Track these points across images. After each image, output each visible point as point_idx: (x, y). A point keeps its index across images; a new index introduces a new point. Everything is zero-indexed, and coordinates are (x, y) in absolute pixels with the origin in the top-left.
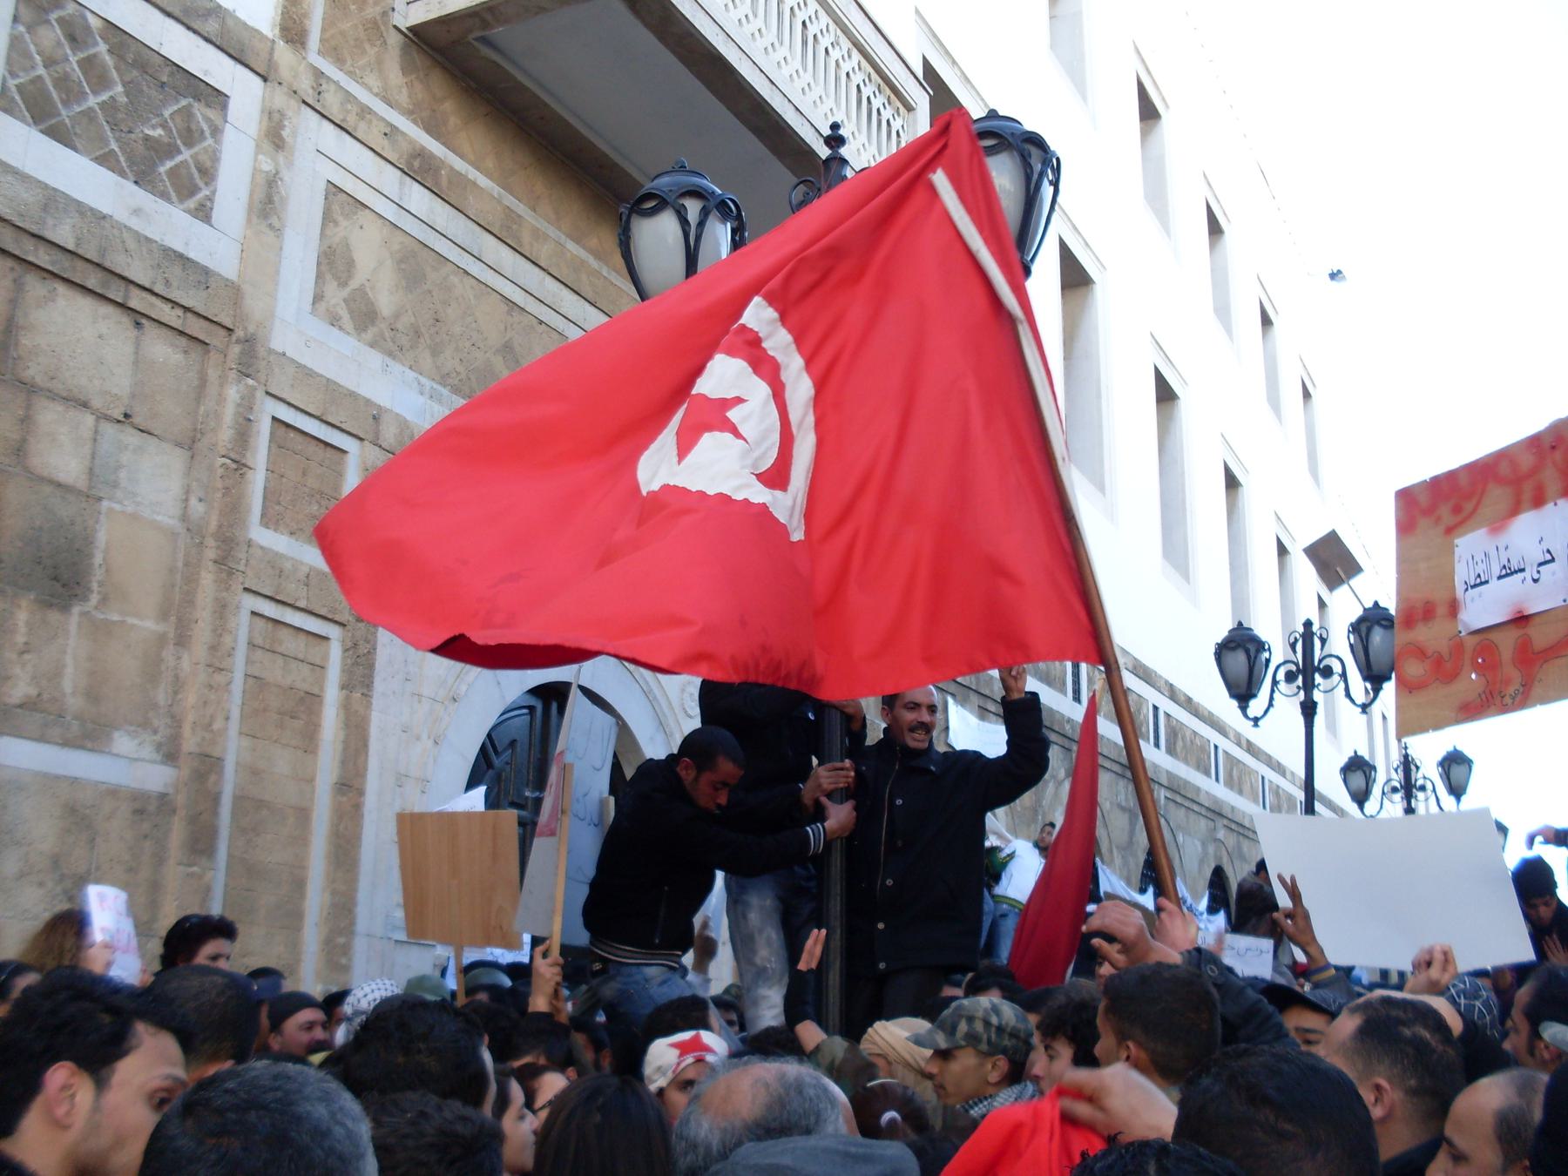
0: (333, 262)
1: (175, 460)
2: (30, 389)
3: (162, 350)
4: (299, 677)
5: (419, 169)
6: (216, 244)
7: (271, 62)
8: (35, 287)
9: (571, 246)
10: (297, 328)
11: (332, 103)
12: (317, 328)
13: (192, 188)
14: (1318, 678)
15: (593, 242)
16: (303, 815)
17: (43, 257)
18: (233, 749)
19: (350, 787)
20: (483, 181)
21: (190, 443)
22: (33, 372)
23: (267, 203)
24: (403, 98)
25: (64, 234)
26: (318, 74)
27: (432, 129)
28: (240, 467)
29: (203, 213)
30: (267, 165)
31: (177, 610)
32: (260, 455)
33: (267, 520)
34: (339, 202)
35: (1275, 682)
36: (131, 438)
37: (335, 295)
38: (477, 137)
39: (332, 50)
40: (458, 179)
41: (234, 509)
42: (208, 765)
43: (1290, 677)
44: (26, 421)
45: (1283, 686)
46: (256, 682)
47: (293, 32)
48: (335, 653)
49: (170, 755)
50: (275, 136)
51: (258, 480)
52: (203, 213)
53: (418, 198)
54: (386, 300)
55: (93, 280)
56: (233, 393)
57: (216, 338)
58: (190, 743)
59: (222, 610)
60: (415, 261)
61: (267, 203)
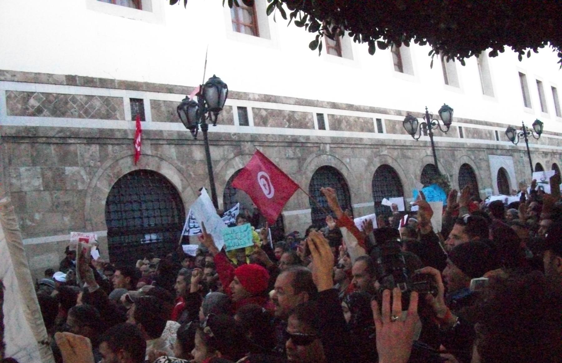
45: (520, 137)
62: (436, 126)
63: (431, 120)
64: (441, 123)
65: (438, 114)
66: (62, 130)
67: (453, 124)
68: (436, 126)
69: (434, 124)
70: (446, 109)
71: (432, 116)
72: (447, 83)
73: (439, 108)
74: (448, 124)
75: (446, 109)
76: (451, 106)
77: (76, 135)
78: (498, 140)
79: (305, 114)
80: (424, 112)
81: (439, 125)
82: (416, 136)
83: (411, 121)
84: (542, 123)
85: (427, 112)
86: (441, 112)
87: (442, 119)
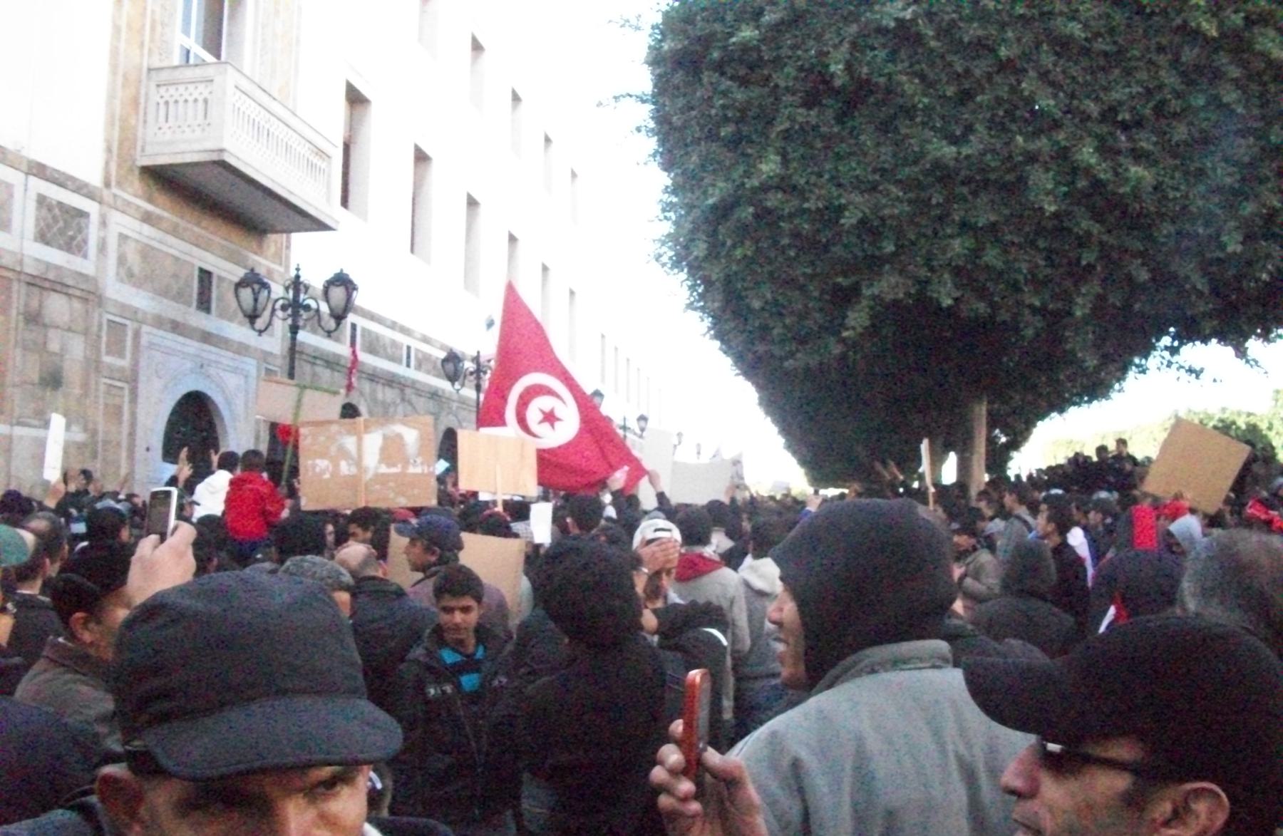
0: (122, 260)
1: (82, 338)
2: (45, 326)
3: (77, 305)
4: (117, 401)
5: (147, 218)
6: (86, 266)
7: (101, 197)
8: (45, 293)
9: (196, 229)
10: (117, 291)
11: (119, 203)
12: (118, 285)
13: (42, 200)
14: (302, 312)
15: (204, 223)
16: (119, 444)
17: (47, 285)
18: (101, 428)
19: (132, 435)
20: (166, 214)
21: (86, 332)
22: (47, 321)
23: (102, 248)
24: (140, 192)
25: (51, 276)
26: (115, 196)
27: (150, 200)
28: (99, 337)
29: (85, 256)
30: (102, 234)
31: (85, 385)
32: (105, 327)
33: (108, 353)
34: (123, 238)
35: (274, 310)
36: (71, 334)
37: (123, 272)
38: (162, 198)
39: (119, 184)
40: (160, 218)
41: (99, 350)
42: (94, 433)
43: (284, 308)
44: (46, 336)
45: (280, 313)
46: (106, 405)
47: (107, 184)
48: (126, 392)
49: (85, 430)
50: (104, 223)
51: (104, 339)
52: (85, 256)
53: (147, 229)
54: (136, 270)
55: (58, 288)
56: (96, 315)
57: (91, 297)
58: (91, 426)
59: (97, 383)
60: (146, 252)
61: (102, 248)
62: (312, 313)
63: (302, 296)
64: (324, 308)
65: (321, 287)
66: (316, 349)
67: (351, 318)
68: (312, 313)
69: (307, 308)
70: (342, 281)
71: (307, 288)
72: (412, 250)
73: (329, 276)
74: (339, 317)
75: (342, 281)
76: (353, 277)
77: (413, 384)
78: (408, 365)
79: (394, 344)
80: (475, 354)
81: (318, 311)
82: (457, 386)
83: (256, 287)
84: (355, 288)
85: (298, 277)
86: (330, 284)
87: (327, 301)
